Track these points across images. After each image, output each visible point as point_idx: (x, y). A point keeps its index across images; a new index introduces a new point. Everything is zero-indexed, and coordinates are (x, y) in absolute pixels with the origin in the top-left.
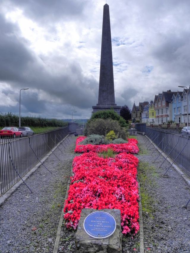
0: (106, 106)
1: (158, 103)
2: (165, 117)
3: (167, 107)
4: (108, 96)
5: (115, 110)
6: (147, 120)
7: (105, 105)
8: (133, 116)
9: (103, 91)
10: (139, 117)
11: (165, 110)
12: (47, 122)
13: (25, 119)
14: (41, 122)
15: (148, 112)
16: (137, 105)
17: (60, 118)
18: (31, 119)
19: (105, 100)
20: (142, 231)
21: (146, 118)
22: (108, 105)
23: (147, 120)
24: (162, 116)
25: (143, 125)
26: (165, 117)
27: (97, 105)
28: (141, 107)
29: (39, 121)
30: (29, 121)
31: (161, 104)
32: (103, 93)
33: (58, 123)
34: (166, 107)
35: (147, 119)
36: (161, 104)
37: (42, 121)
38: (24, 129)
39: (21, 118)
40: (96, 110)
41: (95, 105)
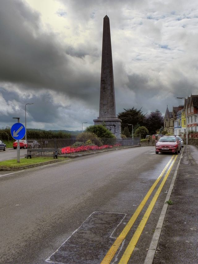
0: (107, 119)
1: (191, 107)
2: (194, 127)
3: (196, 115)
4: (108, 110)
5: (114, 122)
6: (180, 130)
7: (106, 118)
8: (166, 126)
9: (104, 105)
10: (172, 126)
11: (194, 118)
12: (52, 135)
13: (30, 133)
14: (46, 135)
15: (181, 120)
16: (171, 110)
17: (74, 130)
18: (36, 133)
19: (106, 114)
20: (155, 240)
21: (178, 127)
22: (108, 118)
23: (180, 130)
24: (191, 125)
25: (61, 137)
26: (194, 127)
27: (98, 118)
28: (175, 112)
29: (44, 135)
30: (34, 135)
31: (191, 111)
32: (104, 107)
33: (65, 136)
34: (195, 114)
35: (179, 129)
36: (191, 111)
37: (47, 134)
38: (32, 142)
39: (28, 132)
40: (96, 123)
41: (97, 119)
